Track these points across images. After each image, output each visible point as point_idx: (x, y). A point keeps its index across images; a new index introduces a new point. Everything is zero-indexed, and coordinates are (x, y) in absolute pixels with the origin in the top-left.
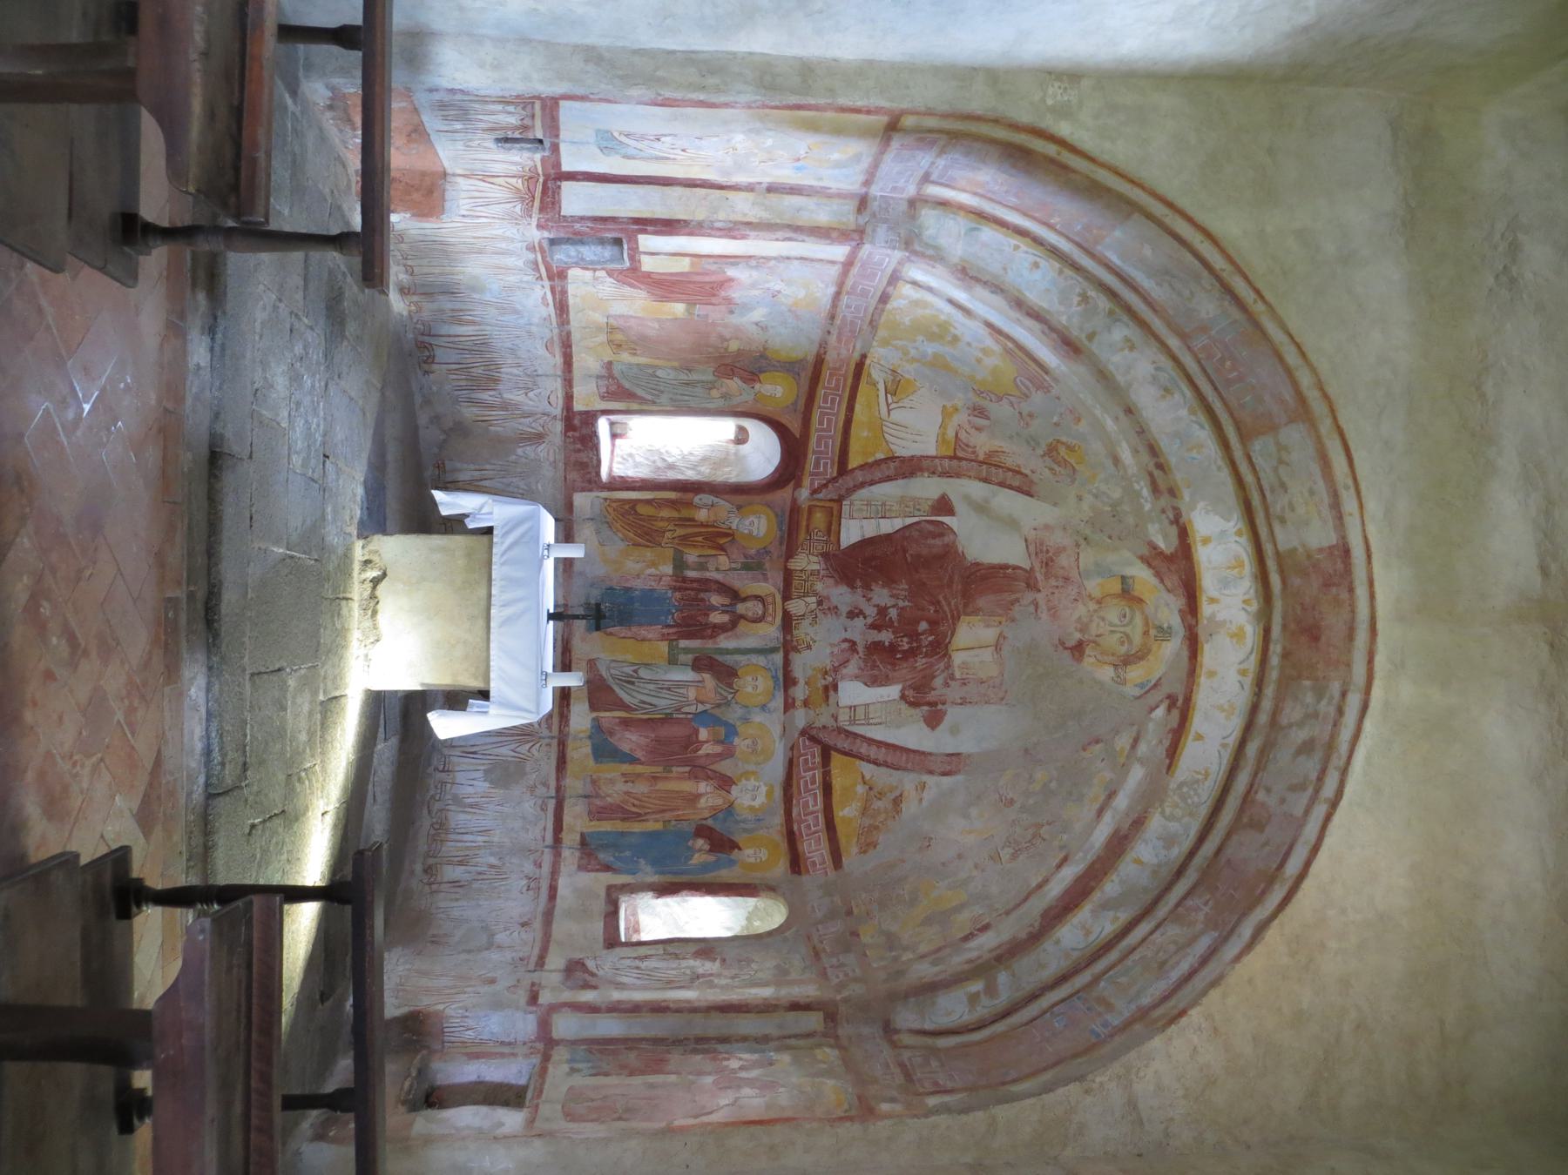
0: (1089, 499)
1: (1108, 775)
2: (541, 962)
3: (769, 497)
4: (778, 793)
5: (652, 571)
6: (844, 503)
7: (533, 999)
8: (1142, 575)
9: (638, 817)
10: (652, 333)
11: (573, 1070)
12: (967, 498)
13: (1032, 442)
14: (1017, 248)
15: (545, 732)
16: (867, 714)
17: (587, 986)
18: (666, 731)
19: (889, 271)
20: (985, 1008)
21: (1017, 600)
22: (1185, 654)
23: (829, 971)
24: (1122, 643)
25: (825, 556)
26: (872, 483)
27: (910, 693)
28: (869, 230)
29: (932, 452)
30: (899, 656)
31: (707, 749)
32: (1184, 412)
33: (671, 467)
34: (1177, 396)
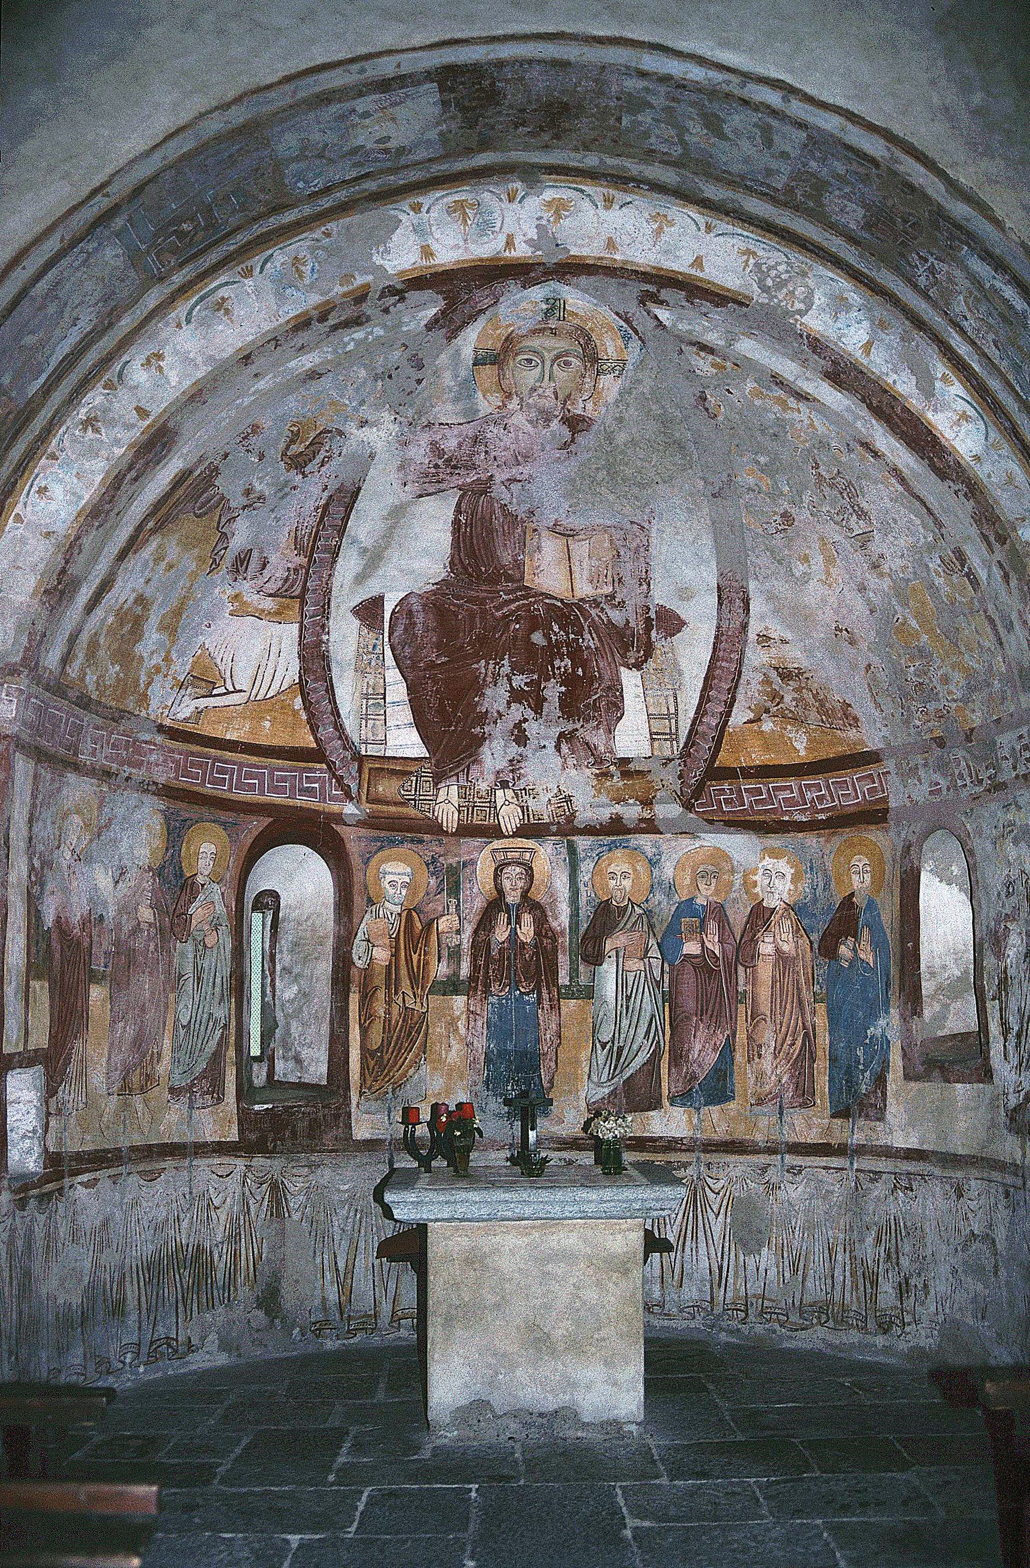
3: (356, 861)
4: (774, 841)
6: (364, 753)
9: (810, 1037)
13: (285, 490)
16: (661, 717)
22: (583, 280)
24: (567, 364)
25: (438, 778)
26: (336, 713)
27: (632, 656)
30: (580, 672)
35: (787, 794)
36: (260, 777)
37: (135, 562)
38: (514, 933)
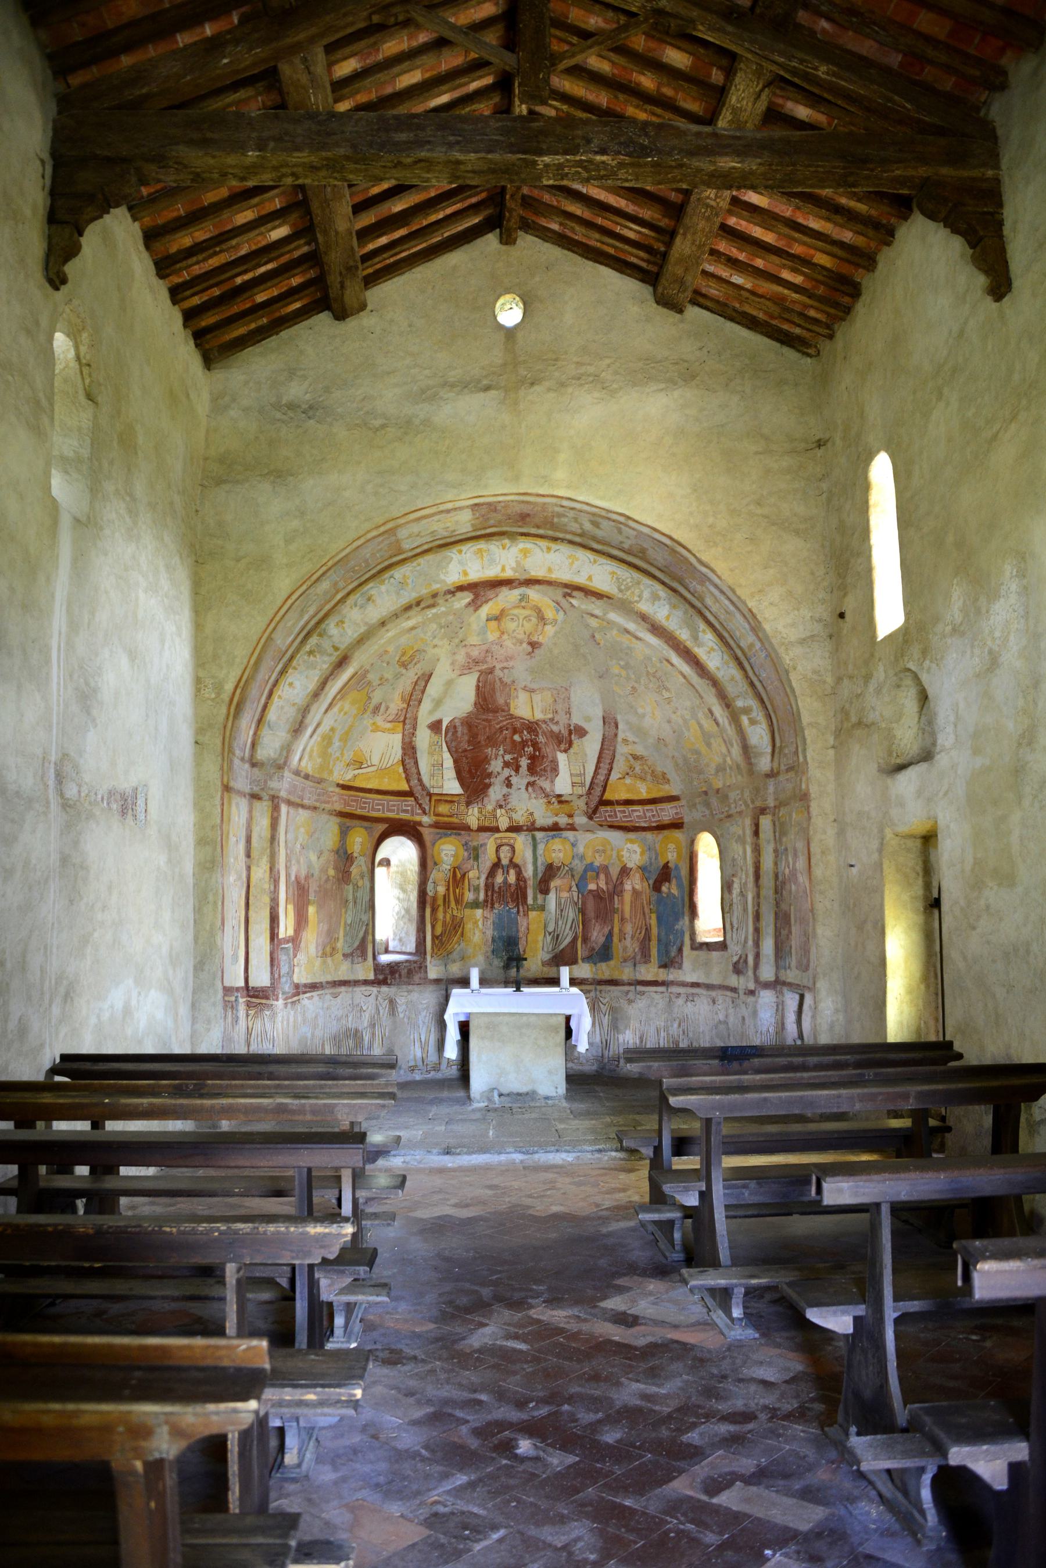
0: (436, 641)
1: (615, 632)
2: (734, 990)
3: (428, 844)
4: (632, 835)
5: (480, 924)
7: (752, 993)
8: (485, 610)
9: (648, 930)
10: (326, 928)
11: (789, 967)
12: (431, 712)
13: (398, 676)
14: (280, 697)
15: (592, 994)
16: (577, 775)
17: (746, 962)
18: (591, 913)
19: (293, 776)
20: (758, 714)
21: (500, 679)
22: (537, 587)
23: (738, 810)
25: (468, 804)
26: (419, 774)
27: (563, 746)
28: (272, 793)
29: (399, 736)
31: (602, 884)
32: (383, 588)
33: (407, 911)
34: (372, 592)
35: (638, 814)
36: (383, 805)
37: (330, 713)
38: (506, 879)
